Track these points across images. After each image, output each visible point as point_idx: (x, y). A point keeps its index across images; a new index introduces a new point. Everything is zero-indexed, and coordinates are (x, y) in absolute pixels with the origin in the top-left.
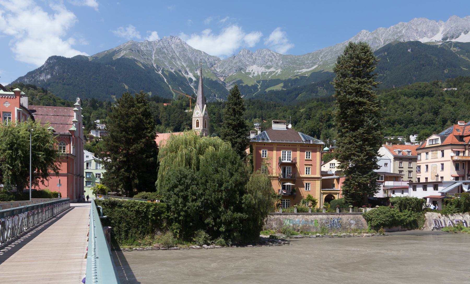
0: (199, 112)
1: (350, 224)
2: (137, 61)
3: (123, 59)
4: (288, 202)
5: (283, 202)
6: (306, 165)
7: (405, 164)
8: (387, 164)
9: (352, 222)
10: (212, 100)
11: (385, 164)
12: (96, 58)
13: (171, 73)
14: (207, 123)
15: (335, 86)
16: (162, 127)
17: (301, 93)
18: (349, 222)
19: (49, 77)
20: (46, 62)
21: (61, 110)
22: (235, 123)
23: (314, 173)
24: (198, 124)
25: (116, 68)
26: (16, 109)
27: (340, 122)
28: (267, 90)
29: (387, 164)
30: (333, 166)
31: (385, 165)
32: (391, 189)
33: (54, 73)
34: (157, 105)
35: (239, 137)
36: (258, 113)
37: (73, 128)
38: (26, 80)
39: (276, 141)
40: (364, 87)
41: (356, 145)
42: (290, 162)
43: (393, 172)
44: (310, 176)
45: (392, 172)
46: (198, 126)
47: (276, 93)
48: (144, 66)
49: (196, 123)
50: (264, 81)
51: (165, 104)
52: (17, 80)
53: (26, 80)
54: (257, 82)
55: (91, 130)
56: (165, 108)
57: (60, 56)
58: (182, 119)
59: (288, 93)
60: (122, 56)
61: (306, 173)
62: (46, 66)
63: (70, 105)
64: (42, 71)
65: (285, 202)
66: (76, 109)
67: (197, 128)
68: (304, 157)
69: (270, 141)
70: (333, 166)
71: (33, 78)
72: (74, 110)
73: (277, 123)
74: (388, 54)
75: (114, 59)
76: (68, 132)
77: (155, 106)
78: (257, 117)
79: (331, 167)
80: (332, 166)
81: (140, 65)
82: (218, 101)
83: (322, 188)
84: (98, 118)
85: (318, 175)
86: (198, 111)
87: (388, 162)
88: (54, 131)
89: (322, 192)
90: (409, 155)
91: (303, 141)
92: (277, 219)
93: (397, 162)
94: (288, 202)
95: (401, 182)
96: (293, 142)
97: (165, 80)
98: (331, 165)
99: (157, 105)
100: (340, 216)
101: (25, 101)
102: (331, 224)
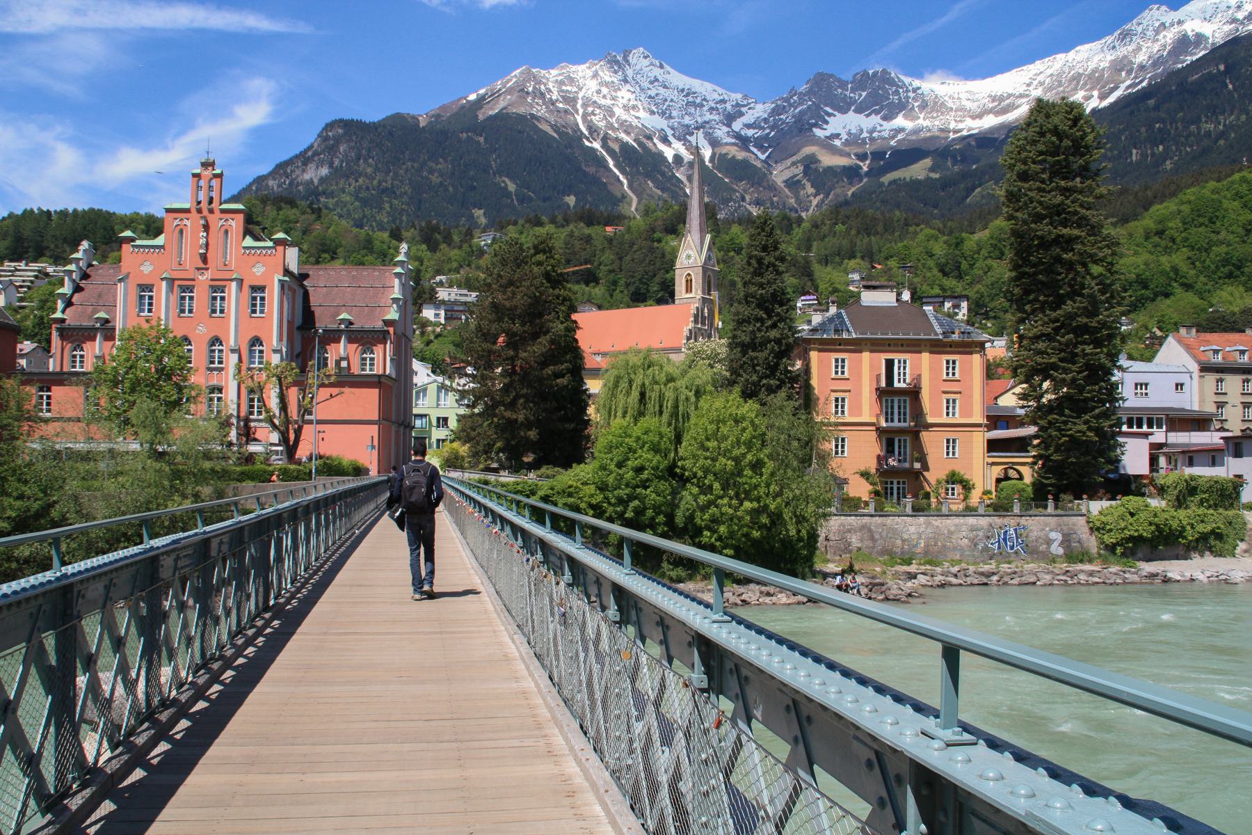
0: (693, 253)
1: (1049, 542)
2: (538, 119)
3: (502, 116)
4: (901, 486)
5: (889, 486)
6: (944, 392)
8: (1182, 385)
9: (1053, 535)
10: (736, 210)
11: (1177, 385)
12: (438, 116)
13: (625, 147)
14: (712, 282)
15: (1002, 199)
16: (598, 291)
17: (980, 185)
18: (1047, 536)
19: (324, 171)
20: (319, 136)
21: (369, 275)
22: (763, 292)
23: (967, 412)
24: (689, 283)
25: (485, 139)
26: (278, 277)
27: (1018, 286)
28: (887, 179)
29: (1182, 385)
30: (1144, 391)
31: (1177, 389)
32: (1183, 452)
33: (337, 162)
34: (587, 231)
35: (774, 326)
36: (859, 243)
37: (393, 314)
38: (271, 183)
39: (869, 336)
40: (1073, 202)
41: (1060, 343)
42: (905, 386)
43: (1200, 406)
44: (848, 419)
45: (1196, 408)
46: (689, 289)
47: (914, 185)
48: (555, 131)
49: (684, 281)
50: (878, 155)
51: (609, 229)
52: (251, 185)
53: (271, 183)
54: (858, 159)
55: (424, 306)
56: (610, 240)
57: (353, 120)
58: (652, 267)
59: (945, 184)
60: (503, 109)
61: (948, 414)
62: (319, 146)
63: (386, 258)
64: (309, 158)
65: (895, 486)
66: (399, 270)
67: (688, 295)
68: (942, 374)
69: (854, 336)
70: (1144, 391)
71: (287, 177)
72: (395, 274)
73: (874, 288)
75: (481, 117)
76: (381, 323)
77: (583, 234)
78: (859, 255)
79: (1136, 394)
80: (1139, 391)
81: (544, 127)
82: (750, 213)
83: (988, 452)
84: (439, 272)
85: (978, 418)
86: (691, 253)
87: (1183, 378)
88: (351, 323)
89: (991, 460)
90: (1242, 361)
91: (936, 334)
92: (863, 527)
93: (1211, 378)
94: (901, 486)
95: (1209, 433)
96: (911, 336)
97: (611, 163)
98: (1136, 389)
99: (587, 231)
100: (1023, 521)
101: (292, 256)
102: (999, 541)
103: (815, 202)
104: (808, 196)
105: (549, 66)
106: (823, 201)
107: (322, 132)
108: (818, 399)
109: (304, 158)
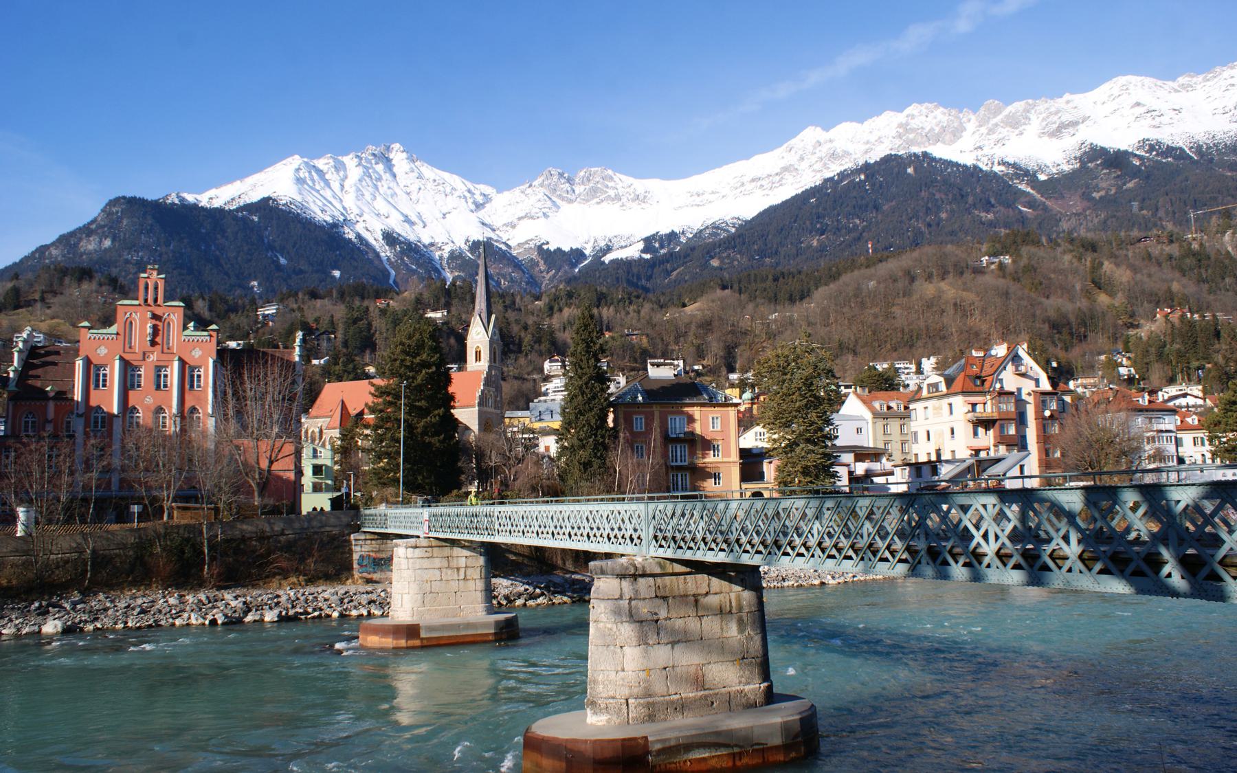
7: (894, 425)
19: (107, 243)
20: (103, 211)
52: (33, 253)
56: (383, 312)
57: (135, 197)
59: (651, 264)
62: (102, 220)
73: (658, 365)
74: (866, 177)
93: (881, 423)
103: (548, 277)
104: (542, 272)
105: (319, 158)
106: (554, 276)
107: (105, 207)
108: (1232, 68)
109: (87, 230)
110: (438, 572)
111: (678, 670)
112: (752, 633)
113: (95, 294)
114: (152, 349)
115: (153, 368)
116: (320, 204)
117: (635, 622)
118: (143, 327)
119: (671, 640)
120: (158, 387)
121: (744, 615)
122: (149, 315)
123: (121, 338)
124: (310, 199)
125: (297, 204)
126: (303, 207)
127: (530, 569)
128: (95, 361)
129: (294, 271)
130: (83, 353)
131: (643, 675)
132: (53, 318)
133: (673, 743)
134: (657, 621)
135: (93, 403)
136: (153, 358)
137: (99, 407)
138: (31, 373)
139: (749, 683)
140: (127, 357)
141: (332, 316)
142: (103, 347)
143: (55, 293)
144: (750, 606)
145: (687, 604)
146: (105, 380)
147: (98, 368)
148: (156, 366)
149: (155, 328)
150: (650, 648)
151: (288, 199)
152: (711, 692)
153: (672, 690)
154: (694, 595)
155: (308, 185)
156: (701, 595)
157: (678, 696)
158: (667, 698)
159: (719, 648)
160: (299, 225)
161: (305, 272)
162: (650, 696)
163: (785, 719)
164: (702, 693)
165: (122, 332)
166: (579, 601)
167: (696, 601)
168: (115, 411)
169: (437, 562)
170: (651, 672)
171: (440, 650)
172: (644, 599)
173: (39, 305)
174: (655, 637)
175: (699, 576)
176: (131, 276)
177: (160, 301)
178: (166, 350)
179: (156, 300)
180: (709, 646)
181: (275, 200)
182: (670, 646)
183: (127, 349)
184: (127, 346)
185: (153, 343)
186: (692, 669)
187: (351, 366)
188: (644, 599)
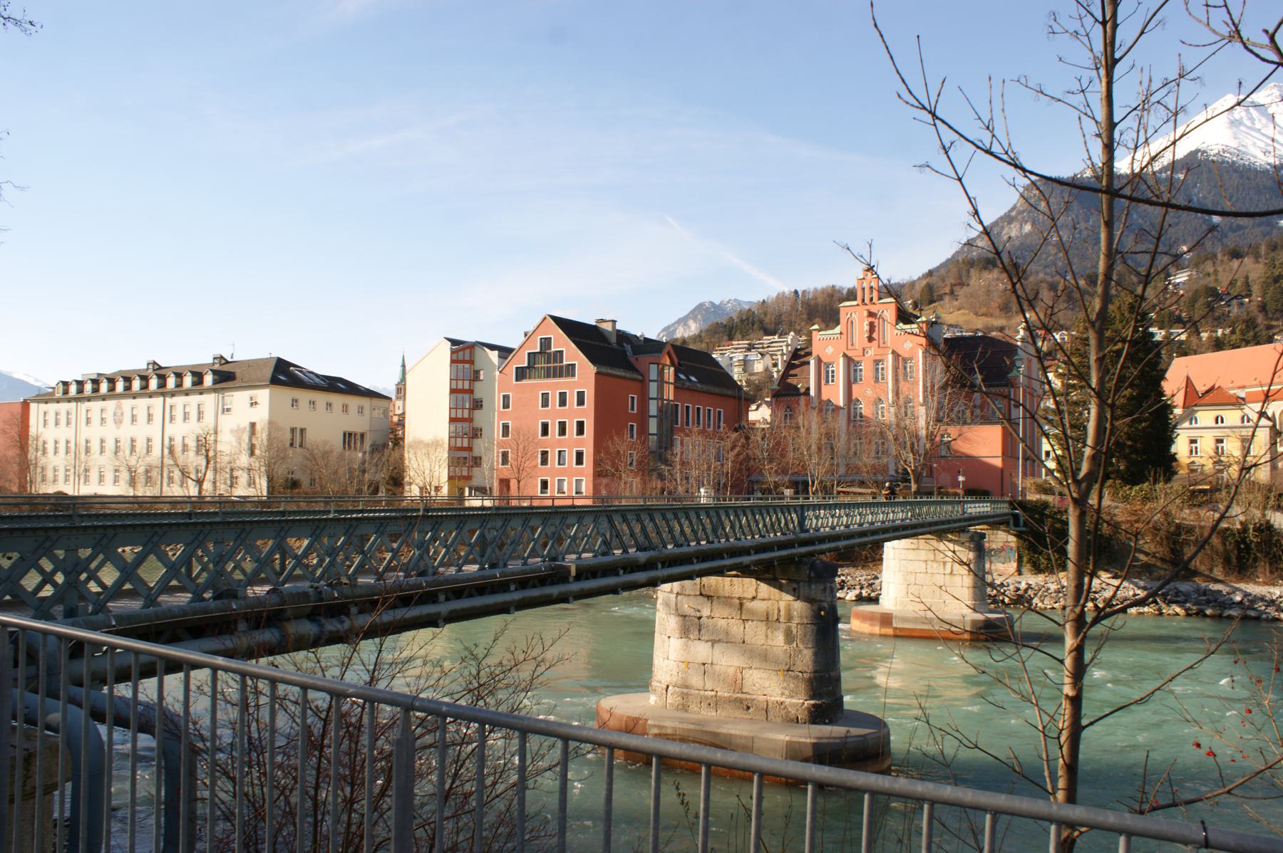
19: (1028, 228)
110: (923, 565)
111: (717, 668)
112: (801, 646)
113: (994, 283)
114: (869, 344)
115: (872, 363)
116: (1262, 145)
117: (679, 615)
118: (861, 322)
119: (712, 638)
120: (877, 379)
121: (793, 625)
122: (866, 313)
123: (844, 337)
124: (1248, 141)
125: (1232, 150)
126: (1239, 153)
127: (1162, 572)
128: (824, 360)
129: (1231, 228)
130: (814, 354)
131: (683, 666)
132: (959, 309)
133: (669, 731)
134: (700, 618)
135: (824, 397)
136: (871, 353)
137: (829, 401)
138: (792, 372)
139: (792, 697)
140: (850, 354)
141: (1247, 278)
142: (830, 347)
143: (962, 284)
144: (801, 617)
145: (731, 605)
146: (833, 376)
147: (828, 365)
148: (875, 361)
149: (872, 326)
150: (690, 642)
151: (1220, 148)
152: (748, 696)
153: (709, 686)
154: (739, 598)
155: (1245, 126)
156: (747, 599)
157: (713, 693)
158: (702, 692)
159: (764, 657)
160: (1235, 175)
161: (1246, 228)
162: (687, 687)
163: (794, 739)
164: (739, 695)
165: (844, 332)
166: (1197, 614)
167: (741, 604)
168: (841, 404)
169: (923, 555)
170: (690, 665)
171: (932, 643)
172: (689, 595)
173: (947, 298)
174: (697, 633)
175: (747, 580)
176: (1051, 258)
177: (875, 300)
178: (881, 345)
179: (871, 299)
180: (752, 651)
181: (1204, 152)
182: (710, 643)
183: (850, 347)
184: (850, 343)
185: (870, 339)
186: (731, 671)
187: (1251, 334)
188: (689, 595)
